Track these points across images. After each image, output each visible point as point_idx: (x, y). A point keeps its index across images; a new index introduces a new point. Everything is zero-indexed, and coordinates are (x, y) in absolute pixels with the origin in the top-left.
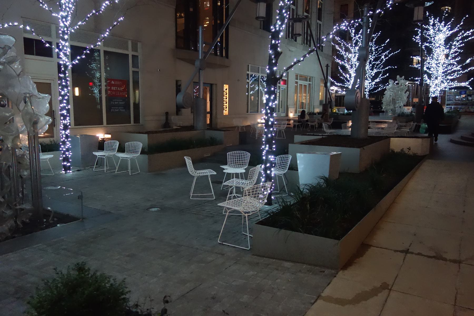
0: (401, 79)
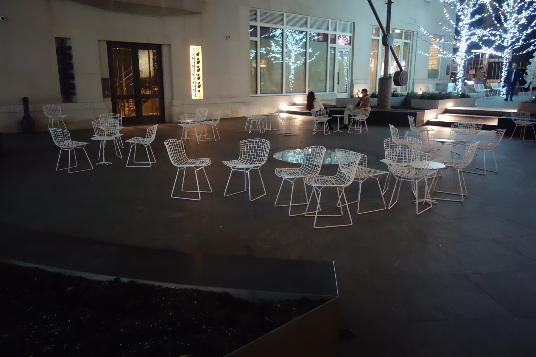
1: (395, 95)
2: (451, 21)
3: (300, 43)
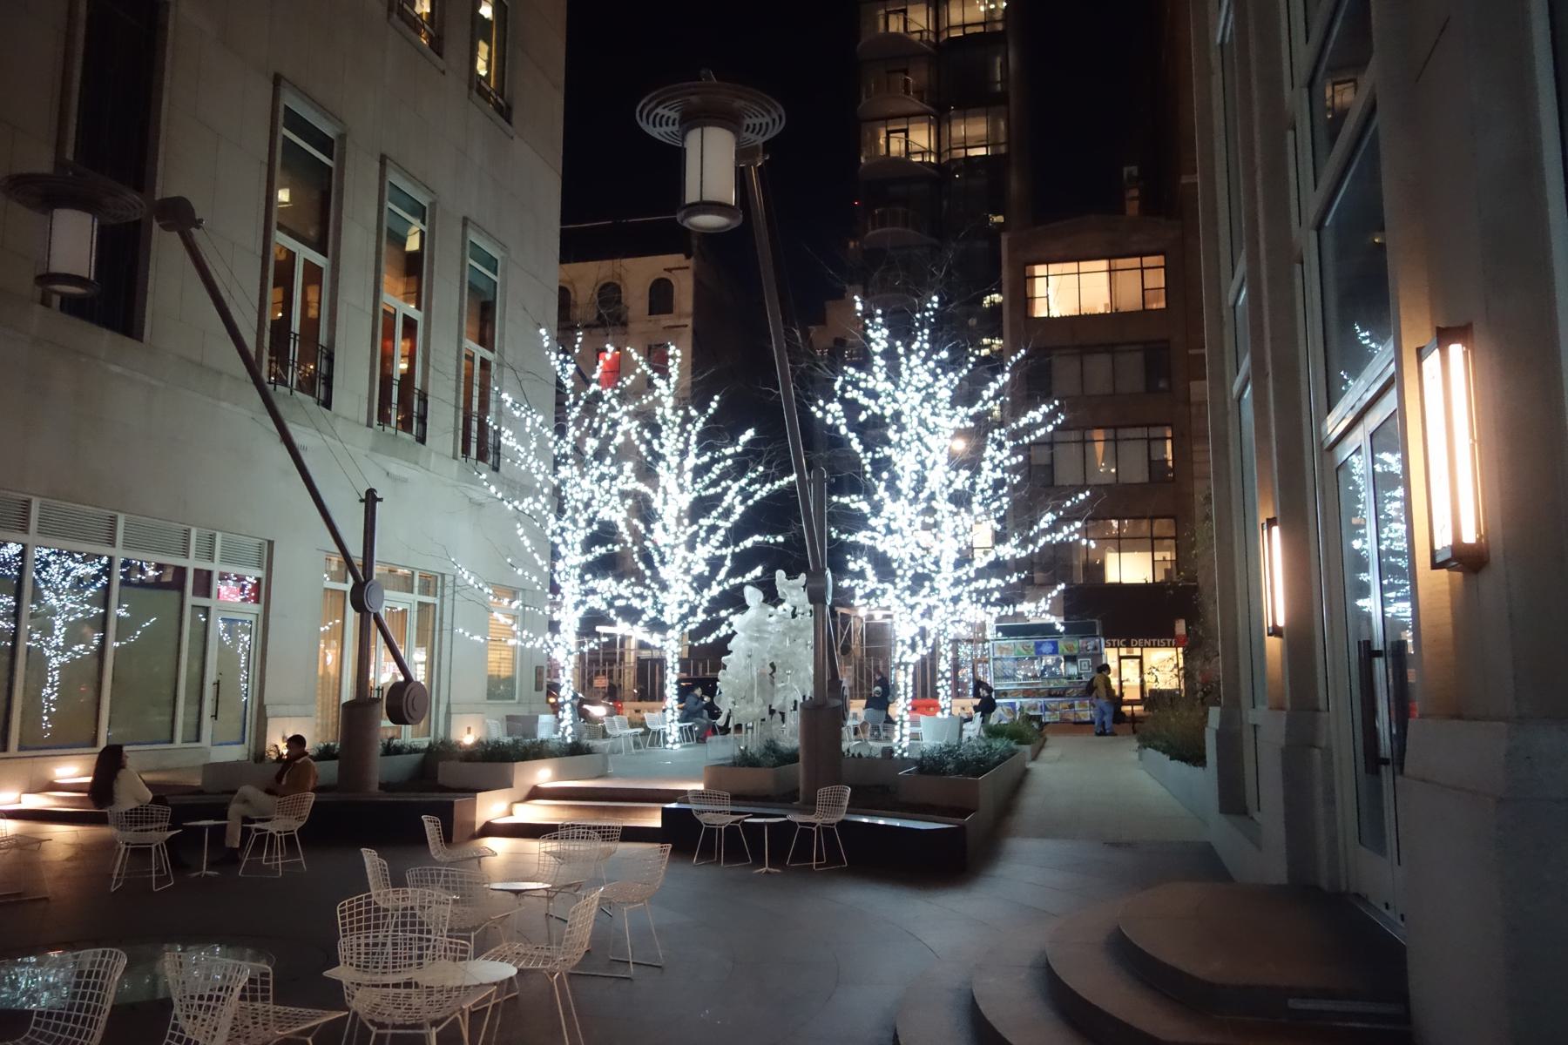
1: (391, 750)
2: (536, 556)
3: (87, 587)
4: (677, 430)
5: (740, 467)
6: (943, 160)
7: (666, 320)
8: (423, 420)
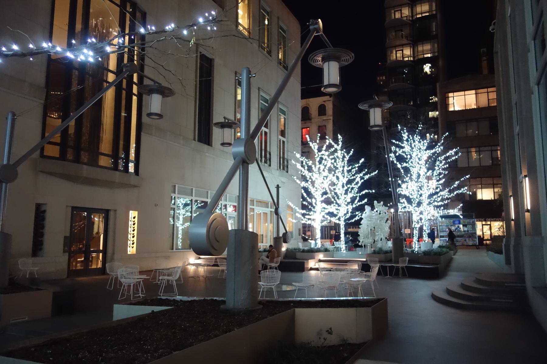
0: (380, 206)
4: (341, 160)
5: (360, 170)
6: (415, 59)
7: (324, 118)
8: (270, 159)
